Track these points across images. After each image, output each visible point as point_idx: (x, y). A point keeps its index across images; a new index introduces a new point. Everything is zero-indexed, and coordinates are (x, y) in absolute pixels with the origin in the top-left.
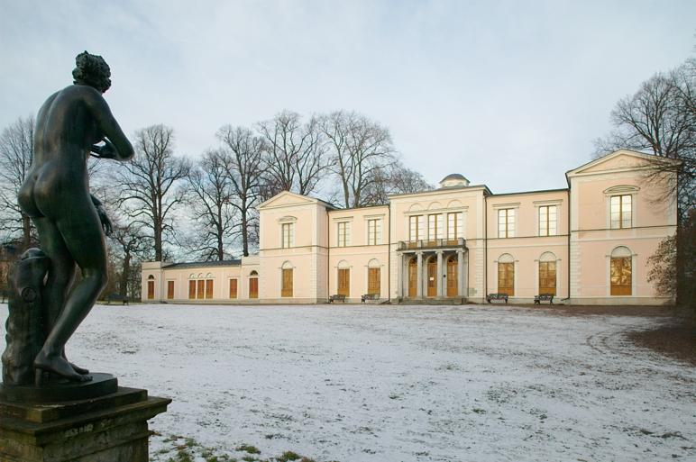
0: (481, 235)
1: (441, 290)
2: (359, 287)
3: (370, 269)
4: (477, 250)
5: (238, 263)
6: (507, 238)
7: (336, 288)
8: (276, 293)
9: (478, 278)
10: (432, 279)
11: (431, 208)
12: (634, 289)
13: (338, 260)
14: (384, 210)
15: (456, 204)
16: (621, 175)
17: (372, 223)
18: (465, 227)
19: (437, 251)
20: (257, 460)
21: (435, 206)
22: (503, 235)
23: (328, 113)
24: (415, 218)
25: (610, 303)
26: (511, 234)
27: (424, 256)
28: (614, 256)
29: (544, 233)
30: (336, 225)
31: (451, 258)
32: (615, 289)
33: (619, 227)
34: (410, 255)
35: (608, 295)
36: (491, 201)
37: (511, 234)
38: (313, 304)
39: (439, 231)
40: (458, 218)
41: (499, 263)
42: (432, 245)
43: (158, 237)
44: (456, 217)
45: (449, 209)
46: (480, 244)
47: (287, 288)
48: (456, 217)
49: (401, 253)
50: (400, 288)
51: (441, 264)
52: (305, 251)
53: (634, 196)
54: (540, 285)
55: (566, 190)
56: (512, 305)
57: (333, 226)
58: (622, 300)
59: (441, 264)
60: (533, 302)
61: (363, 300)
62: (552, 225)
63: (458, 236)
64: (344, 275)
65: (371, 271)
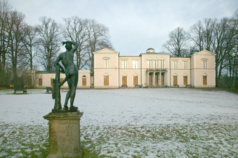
1: (160, 83)
2: (130, 83)
3: (203, 76)
4: (169, 70)
7: (161, 84)
8: (102, 84)
9: (169, 81)
12: (208, 84)
16: (205, 56)
22: (105, 67)
23: (91, 18)
24: (155, 61)
28: (105, 75)
29: (123, 68)
33: (135, 68)
35: (82, 85)
37: (137, 68)
38: (117, 88)
42: (157, 70)
44: (161, 62)
46: (169, 70)
47: (106, 81)
48: (161, 62)
51: (160, 76)
52: (114, 70)
54: (104, 82)
58: (205, 86)
59: (160, 76)
60: (215, 87)
61: (122, 87)
62: (123, 64)
63: (153, 68)
64: (125, 79)
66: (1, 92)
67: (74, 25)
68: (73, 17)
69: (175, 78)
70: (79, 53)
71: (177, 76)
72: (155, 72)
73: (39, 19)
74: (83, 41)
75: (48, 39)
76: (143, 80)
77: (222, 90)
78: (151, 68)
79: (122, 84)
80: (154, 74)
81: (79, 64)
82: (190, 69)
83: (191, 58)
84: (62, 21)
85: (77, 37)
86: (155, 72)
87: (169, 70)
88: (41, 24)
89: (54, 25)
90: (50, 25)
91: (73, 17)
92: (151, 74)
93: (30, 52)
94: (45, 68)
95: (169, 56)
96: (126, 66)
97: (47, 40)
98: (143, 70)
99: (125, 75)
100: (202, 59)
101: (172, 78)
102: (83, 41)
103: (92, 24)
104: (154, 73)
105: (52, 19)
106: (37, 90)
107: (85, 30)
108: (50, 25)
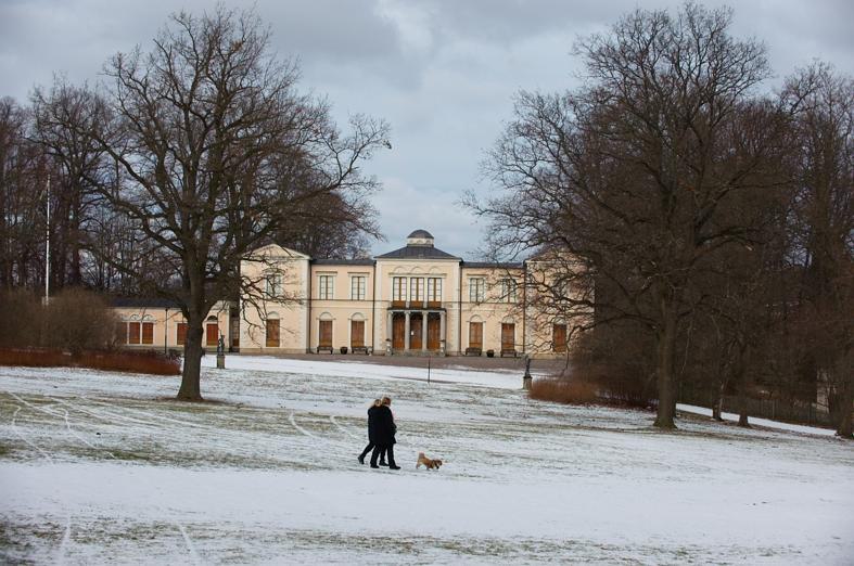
0: (456, 299)
2: (341, 337)
9: (455, 336)
13: (322, 310)
14: (370, 269)
15: (436, 271)
17: (356, 280)
19: (406, 312)
20: (23, 562)
21: (401, 271)
27: (429, 315)
31: (435, 319)
34: (397, 313)
36: (465, 271)
39: (403, 292)
42: (416, 305)
43: (499, 266)
46: (456, 306)
49: (392, 312)
50: (47, 399)
57: (316, 279)
60: (304, 352)
64: (326, 326)
65: (275, 338)
66: (6, 370)
69: (477, 328)
71: (481, 324)
76: (378, 334)
77: (141, 371)
79: (318, 344)
87: (376, 299)
92: (398, 318)
95: (456, 265)
98: (378, 305)
99: (326, 317)
101: (466, 328)
104: (425, 313)
106: (370, 361)
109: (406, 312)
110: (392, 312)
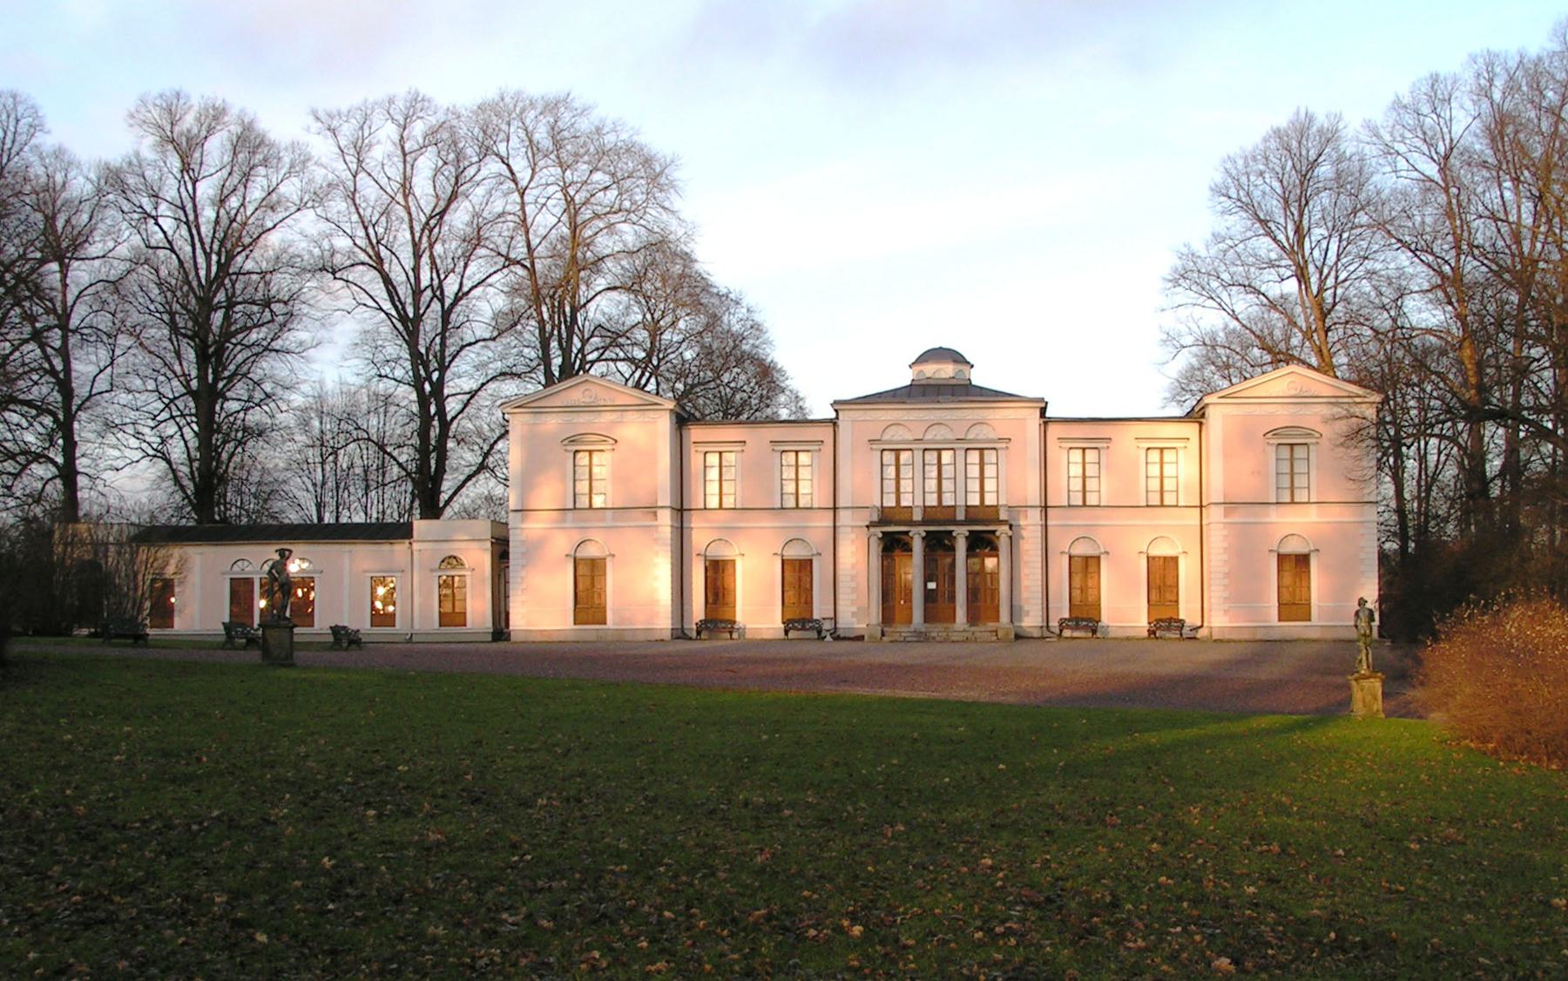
0: (1034, 497)
4: (1030, 524)
5: (402, 531)
6: (797, 507)
10: (932, 585)
11: (929, 437)
18: (1005, 483)
24: (977, 453)
25: (1276, 635)
26: (598, 502)
30: (1143, 453)
31: (982, 543)
32: (444, 619)
33: (1288, 500)
37: (729, 502)
40: (986, 459)
41: (1280, 556)
44: (897, 459)
45: (971, 441)
46: (1035, 517)
48: (897, 459)
49: (878, 531)
53: (1181, 452)
55: (831, 421)
56: (845, 639)
64: (718, 570)
67: (398, 160)
68: (391, 101)
70: (435, 376)
72: (922, 530)
73: (135, 119)
74: (467, 285)
75: (201, 260)
78: (945, 503)
80: (918, 546)
81: (441, 469)
82: (1046, 507)
83: (1201, 424)
84: (308, 129)
85: (417, 256)
86: (922, 530)
88: (147, 147)
89: (250, 148)
90: (216, 150)
91: (391, 101)
92: (893, 545)
93: (58, 364)
94: (178, 497)
96: (974, 471)
97: (189, 265)
98: (844, 518)
100: (1275, 432)
101: (1060, 568)
102: (467, 285)
103: (541, 135)
104: (961, 533)
105: (234, 111)
107: (485, 195)
108: (216, 150)
109: (913, 530)
110: (878, 531)
